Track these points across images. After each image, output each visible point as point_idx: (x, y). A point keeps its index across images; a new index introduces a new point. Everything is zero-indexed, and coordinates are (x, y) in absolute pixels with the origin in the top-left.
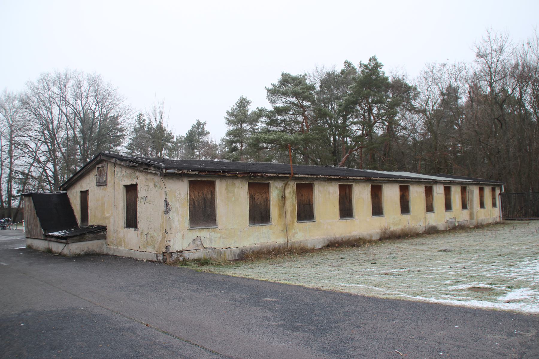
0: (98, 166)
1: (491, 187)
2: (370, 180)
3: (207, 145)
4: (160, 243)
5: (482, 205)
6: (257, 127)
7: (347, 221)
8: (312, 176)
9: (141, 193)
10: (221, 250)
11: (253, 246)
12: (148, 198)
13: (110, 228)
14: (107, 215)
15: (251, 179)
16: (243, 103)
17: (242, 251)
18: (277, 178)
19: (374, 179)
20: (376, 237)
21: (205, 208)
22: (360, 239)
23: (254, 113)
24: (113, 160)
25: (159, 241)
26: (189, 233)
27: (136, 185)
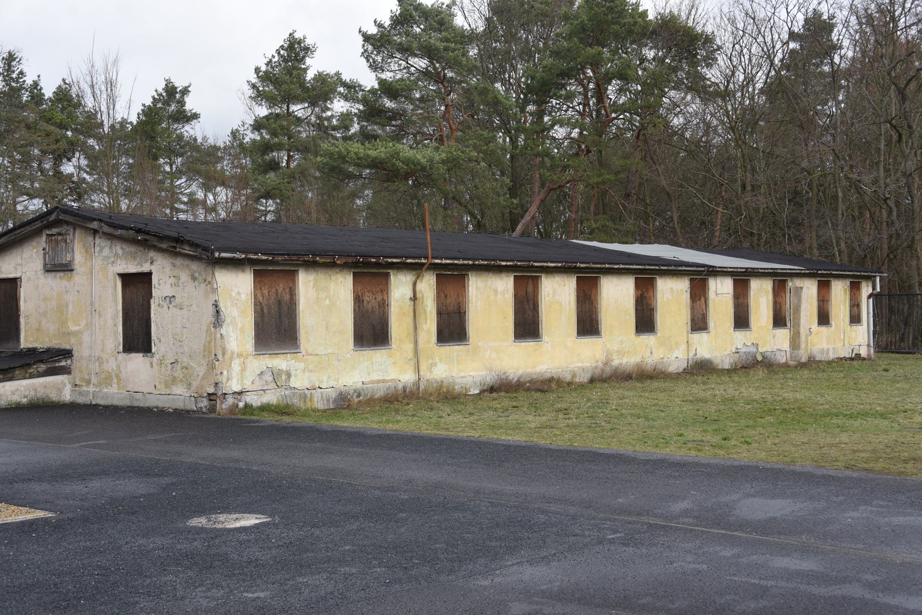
0: (49, 232)
1: (847, 282)
2: (575, 267)
3: (193, 145)
4: (203, 378)
5: (824, 318)
6: (329, 113)
7: (528, 345)
8: (466, 262)
9: (161, 287)
10: (306, 392)
11: (359, 385)
12: (178, 300)
13: (82, 352)
14: (73, 328)
15: (359, 267)
16: (295, 51)
17: (341, 394)
18: (402, 267)
19: (582, 265)
20: (584, 378)
21: (280, 317)
22: (551, 380)
23: (321, 78)
24: (95, 225)
25: (201, 374)
26: (254, 360)
27: (149, 275)
